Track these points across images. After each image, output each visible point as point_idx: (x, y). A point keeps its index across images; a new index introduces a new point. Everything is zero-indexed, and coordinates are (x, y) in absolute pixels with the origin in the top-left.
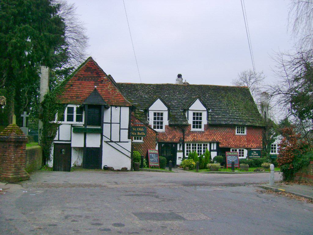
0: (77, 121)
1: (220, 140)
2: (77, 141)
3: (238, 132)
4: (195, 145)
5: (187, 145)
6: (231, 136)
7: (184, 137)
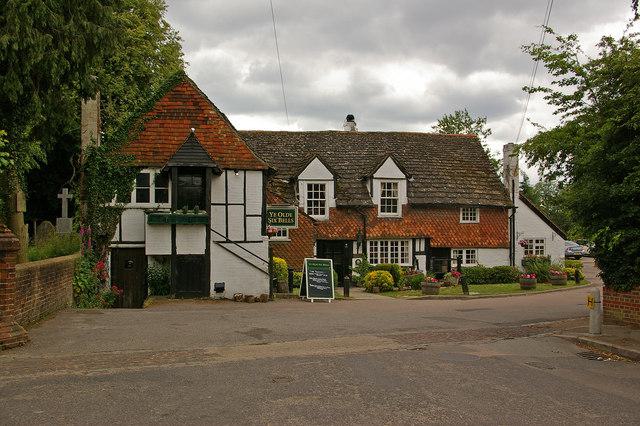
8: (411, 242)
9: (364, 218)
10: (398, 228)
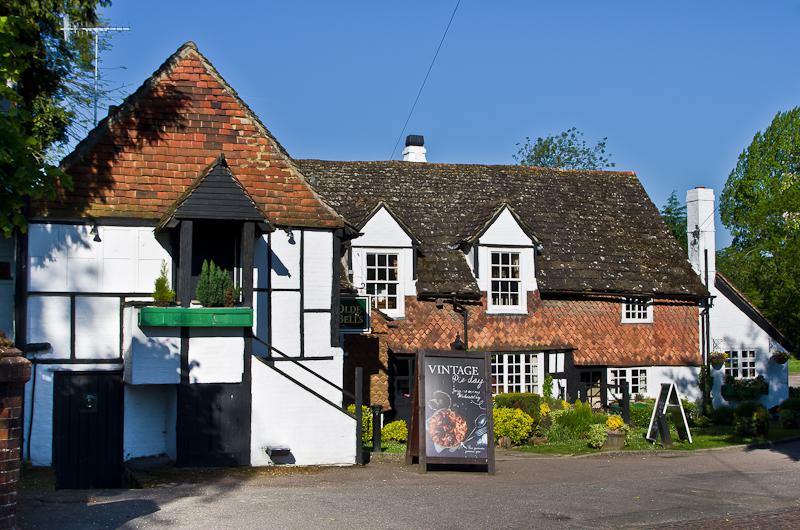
1: (576, 340)
3: (628, 316)
6: (609, 328)
8: (541, 356)
9: (463, 313)
10: (521, 330)
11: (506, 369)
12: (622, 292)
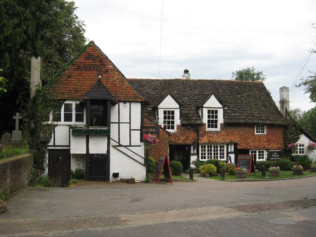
0: (77, 120)
2: (78, 147)
3: (257, 132)
4: (211, 147)
5: (202, 147)
7: (198, 138)
11: (213, 150)
12: (255, 124)
